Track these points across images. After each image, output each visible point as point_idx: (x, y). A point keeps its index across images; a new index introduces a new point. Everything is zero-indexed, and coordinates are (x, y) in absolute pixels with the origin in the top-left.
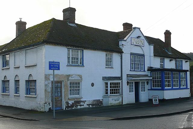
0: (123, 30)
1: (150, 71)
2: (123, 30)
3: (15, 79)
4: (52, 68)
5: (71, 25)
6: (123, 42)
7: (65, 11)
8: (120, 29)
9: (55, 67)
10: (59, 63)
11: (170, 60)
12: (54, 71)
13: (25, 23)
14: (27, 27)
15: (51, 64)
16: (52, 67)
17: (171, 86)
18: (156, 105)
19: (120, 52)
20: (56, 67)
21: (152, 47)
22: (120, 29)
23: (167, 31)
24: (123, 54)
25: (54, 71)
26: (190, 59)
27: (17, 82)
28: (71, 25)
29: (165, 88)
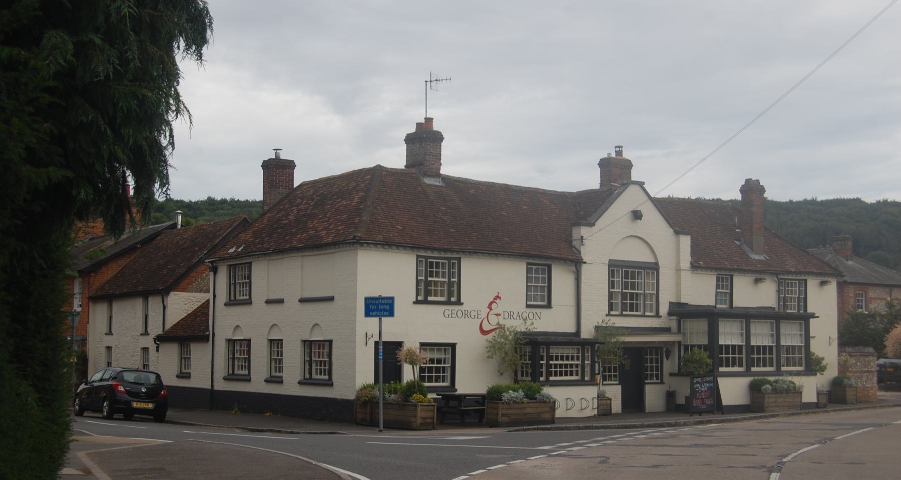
1: (675, 317)
4: (374, 314)
5: (427, 181)
8: (592, 181)
10: (392, 299)
11: (757, 281)
14: (299, 178)
15: (370, 304)
16: (373, 311)
18: (616, 414)
19: (576, 262)
20: (385, 310)
21: (686, 241)
22: (592, 181)
23: (748, 181)
24: (584, 268)
27: (276, 345)
28: (427, 181)
29: (721, 369)
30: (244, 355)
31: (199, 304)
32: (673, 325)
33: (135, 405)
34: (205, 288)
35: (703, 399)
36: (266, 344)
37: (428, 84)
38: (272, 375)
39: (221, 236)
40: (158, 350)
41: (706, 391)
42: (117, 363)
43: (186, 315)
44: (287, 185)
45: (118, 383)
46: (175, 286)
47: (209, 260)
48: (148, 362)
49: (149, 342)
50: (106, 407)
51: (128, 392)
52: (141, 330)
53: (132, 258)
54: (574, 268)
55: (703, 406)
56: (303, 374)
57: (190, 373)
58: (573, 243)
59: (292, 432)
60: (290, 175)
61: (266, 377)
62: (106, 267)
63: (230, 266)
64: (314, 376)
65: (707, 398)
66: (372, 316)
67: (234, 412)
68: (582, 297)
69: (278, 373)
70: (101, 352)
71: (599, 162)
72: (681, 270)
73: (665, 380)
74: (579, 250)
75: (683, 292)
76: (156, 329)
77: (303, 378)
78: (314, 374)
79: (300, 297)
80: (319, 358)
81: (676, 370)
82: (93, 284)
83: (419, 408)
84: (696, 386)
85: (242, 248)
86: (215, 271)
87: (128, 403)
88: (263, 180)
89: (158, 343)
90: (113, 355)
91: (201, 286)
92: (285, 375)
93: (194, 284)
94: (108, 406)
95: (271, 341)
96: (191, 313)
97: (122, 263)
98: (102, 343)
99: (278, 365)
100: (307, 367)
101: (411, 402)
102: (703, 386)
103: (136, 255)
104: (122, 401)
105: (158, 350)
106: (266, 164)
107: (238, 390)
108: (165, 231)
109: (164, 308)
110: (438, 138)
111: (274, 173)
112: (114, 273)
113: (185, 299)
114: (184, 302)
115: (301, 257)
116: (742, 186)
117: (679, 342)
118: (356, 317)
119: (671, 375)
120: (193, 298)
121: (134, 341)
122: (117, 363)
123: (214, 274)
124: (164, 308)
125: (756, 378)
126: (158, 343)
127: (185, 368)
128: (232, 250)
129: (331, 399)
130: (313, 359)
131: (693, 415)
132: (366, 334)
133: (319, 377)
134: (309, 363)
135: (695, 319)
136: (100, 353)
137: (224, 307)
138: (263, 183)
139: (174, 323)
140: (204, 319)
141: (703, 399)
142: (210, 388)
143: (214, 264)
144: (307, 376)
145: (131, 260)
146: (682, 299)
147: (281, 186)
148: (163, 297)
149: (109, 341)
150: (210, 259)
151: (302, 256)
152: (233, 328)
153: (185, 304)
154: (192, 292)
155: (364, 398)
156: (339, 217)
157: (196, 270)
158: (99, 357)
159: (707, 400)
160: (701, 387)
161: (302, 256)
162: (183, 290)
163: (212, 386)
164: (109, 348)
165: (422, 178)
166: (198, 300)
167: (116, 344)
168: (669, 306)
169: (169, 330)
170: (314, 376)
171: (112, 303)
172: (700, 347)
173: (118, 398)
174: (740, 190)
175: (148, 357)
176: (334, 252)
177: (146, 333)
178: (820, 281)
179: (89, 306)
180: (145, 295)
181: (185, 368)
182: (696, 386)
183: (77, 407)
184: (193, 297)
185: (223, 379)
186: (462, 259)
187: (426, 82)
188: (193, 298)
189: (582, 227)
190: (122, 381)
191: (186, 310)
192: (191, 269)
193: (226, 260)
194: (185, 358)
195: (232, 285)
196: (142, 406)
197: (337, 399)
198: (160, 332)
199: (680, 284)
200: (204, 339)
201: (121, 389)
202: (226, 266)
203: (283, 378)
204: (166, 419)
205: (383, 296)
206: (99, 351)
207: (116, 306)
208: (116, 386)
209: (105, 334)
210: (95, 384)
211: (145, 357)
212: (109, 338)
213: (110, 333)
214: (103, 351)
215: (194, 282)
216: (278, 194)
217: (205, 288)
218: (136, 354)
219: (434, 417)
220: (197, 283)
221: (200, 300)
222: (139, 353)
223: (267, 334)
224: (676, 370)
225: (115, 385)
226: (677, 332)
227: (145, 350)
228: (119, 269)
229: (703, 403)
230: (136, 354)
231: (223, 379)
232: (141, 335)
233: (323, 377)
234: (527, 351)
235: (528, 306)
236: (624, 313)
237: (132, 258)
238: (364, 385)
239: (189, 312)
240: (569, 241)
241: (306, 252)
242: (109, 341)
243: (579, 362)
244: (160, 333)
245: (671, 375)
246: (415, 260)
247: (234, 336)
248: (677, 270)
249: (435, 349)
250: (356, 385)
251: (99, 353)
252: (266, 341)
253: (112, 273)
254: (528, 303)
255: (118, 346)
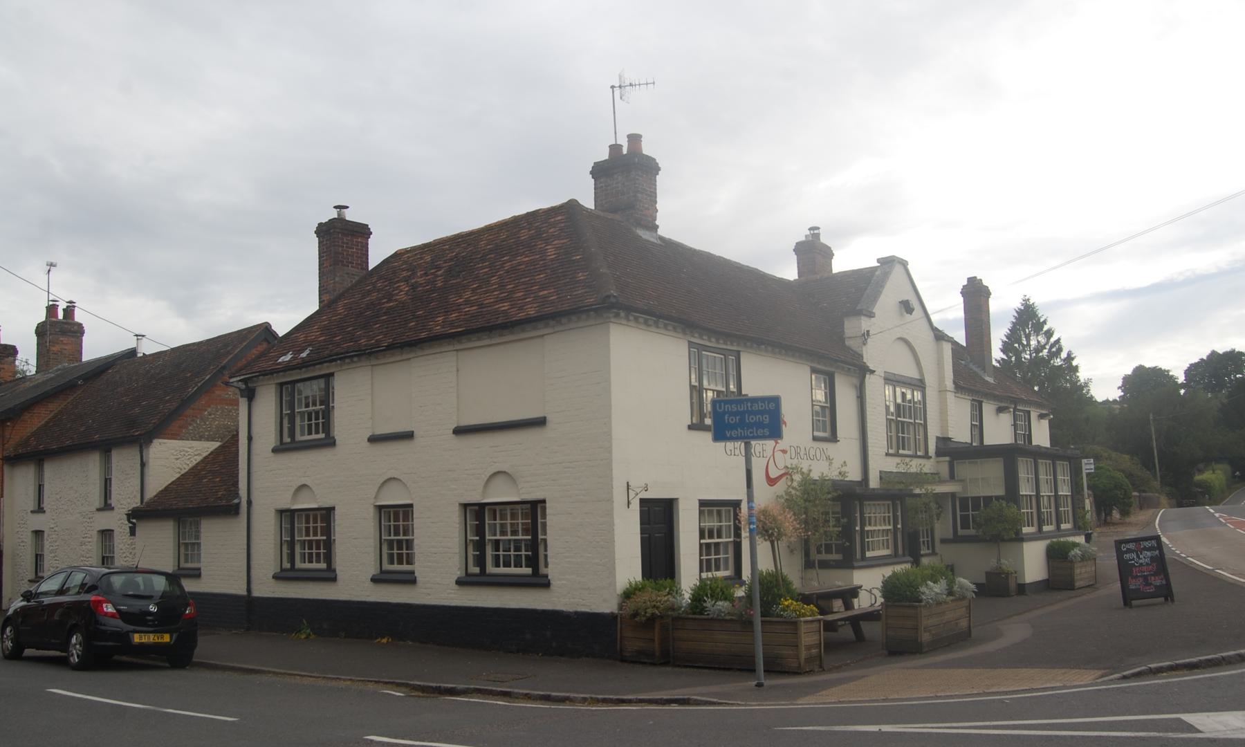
0: (797, 278)
1: (947, 459)
2: (797, 278)
3: (375, 498)
4: (734, 433)
6: (865, 324)
7: (599, 171)
9: (750, 426)
12: (748, 446)
13: (361, 232)
14: (378, 252)
15: (724, 413)
16: (733, 427)
17: (1071, 520)
20: (760, 425)
25: (748, 446)
26: (700, 422)
30: (1065, 511)
31: (199, 458)
32: (944, 470)
33: (137, 638)
34: (207, 433)
35: (1145, 578)
36: (372, 514)
37: (617, 91)
38: (383, 569)
39: (231, 354)
40: (133, 532)
41: (1147, 564)
42: (53, 555)
43: (178, 475)
44: (359, 262)
45: (100, 598)
46: (161, 428)
47: (238, 378)
48: (42, 550)
49: (116, 521)
50: (78, 646)
51: (121, 614)
52: (97, 501)
53: (69, 400)
54: (856, 381)
55: (1148, 588)
56: (464, 566)
57: (199, 569)
58: (846, 343)
59: (549, 696)
60: (362, 247)
61: (374, 573)
62: (30, 413)
63: (281, 385)
64: (299, 565)
65: (1152, 575)
66: (731, 439)
67: (303, 637)
68: (868, 425)
69: (307, 564)
70: (25, 540)
71: (795, 246)
72: (947, 390)
73: (937, 550)
74: (860, 353)
75: (951, 422)
76: (126, 496)
77: (464, 572)
78: (490, 566)
79: (456, 426)
80: (308, 534)
81: (950, 535)
82: (10, 438)
83: (803, 628)
84: (1127, 556)
85: (307, 352)
86: (250, 395)
87: (125, 637)
88: (319, 254)
89: (134, 521)
90: (47, 544)
91: (201, 430)
92: (419, 568)
93: (190, 428)
94: (80, 644)
95: (380, 508)
96: (187, 473)
97: (54, 407)
98: (26, 526)
99: (307, 551)
100: (285, 550)
101: (781, 616)
102: (1141, 556)
103: (75, 396)
104: (109, 632)
105: (133, 532)
106: (324, 228)
107: (305, 597)
108: (119, 362)
109: (143, 465)
110: (650, 168)
111: (340, 241)
112: (43, 422)
113: (177, 451)
114: (174, 455)
115: (455, 352)
116: (964, 286)
117: (953, 495)
118: (610, 452)
119: (943, 541)
120: (189, 450)
121: (85, 520)
122: (53, 555)
123: (248, 401)
124: (143, 465)
125: (1054, 540)
126: (134, 521)
127: (186, 561)
128: (288, 357)
129: (544, 612)
130: (296, 538)
131: (333, 567)
132: (628, 485)
133: (307, 565)
134: (288, 545)
135: (991, 459)
136: (22, 542)
137: (272, 454)
138: (319, 258)
139: (160, 489)
140: (218, 480)
141: (1145, 578)
142: (245, 593)
143: (249, 385)
144: (287, 565)
145: (68, 403)
146: (950, 433)
147: (351, 263)
148: (141, 447)
149: (38, 522)
150: (240, 376)
151: (457, 350)
152: (294, 490)
153: (177, 459)
154: (188, 440)
155: (650, 611)
156: (528, 279)
157: (192, 406)
158: (20, 547)
159: (1153, 578)
160: (1138, 557)
161: (457, 350)
162: (174, 436)
163: (249, 590)
164: (38, 534)
165: (634, 229)
166: (196, 453)
167: (52, 526)
168: (937, 443)
169: (148, 504)
170: (299, 565)
171: (43, 465)
172: (998, 498)
173: (103, 628)
174: (961, 293)
175: (110, 546)
176: (543, 336)
177: (107, 507)
178: (1038, 414)
179: (3, 471)
180: (105, 448)
181: (186, 561)
182: (1127, 556)
183: (9, 644)
184: (190, 448)
185: (273, 577)
186: (741, 353)
187: (613, 87)
188: (189, 450)
189: (863, 317)
190: (109, 591)
191: (179, 468)
192: (185, 403)
193: (275, 375)
194: (186, 545)
195: (287, 419)
196: (151, 640)
197: (563, 611)
198: (136, 503)
199: (947, 412)
200: (230, 510)
201: (109, 608)
202: (274, 386)
203: (549, 577)
204: (195, 660)
205: (749, 395)
206: (19, 538)
207: (49, 469)
208: (99, 603)
209: (32, 512)
210: (47, 600)
211: (106, 546)
212: (40, 516)
213: (40, 509)
214: (28, 539)
215: (190, 425)
216: (346, 276)
217: (207, 433)
218: (90, 540)
219: (821, 644)
220: (195, 425)
221: (199, 452)
222: (95, 538)
223: (374, 496)
224: (950, 535)
225: (94, 601)
226: (948, 479)
227: (106, 534)
228: (50, 416)
229: (1148, 584)
230: (90, 540)
231: (273, 577)
232: (99, 510)
233: (314, 565)
234: (830, 511)
235: (815, 439)
236: (901, 452)
237: (69, 400)
238: (630, 583)
239: (183, 472)
240: (839, 338)
241: (469, 340)
242: (38, 522)
243: (891, 527)
244: (135, 506)
245: (943, 541)
246: (688, 350)
247: (293, 504)
248: (940, 391)
249: (706, 512)
250: (617, 584)
251: (20, 540)
252: (372, 510)
253: (40, 422)
254: (816, 434)
255: (56, 529)
